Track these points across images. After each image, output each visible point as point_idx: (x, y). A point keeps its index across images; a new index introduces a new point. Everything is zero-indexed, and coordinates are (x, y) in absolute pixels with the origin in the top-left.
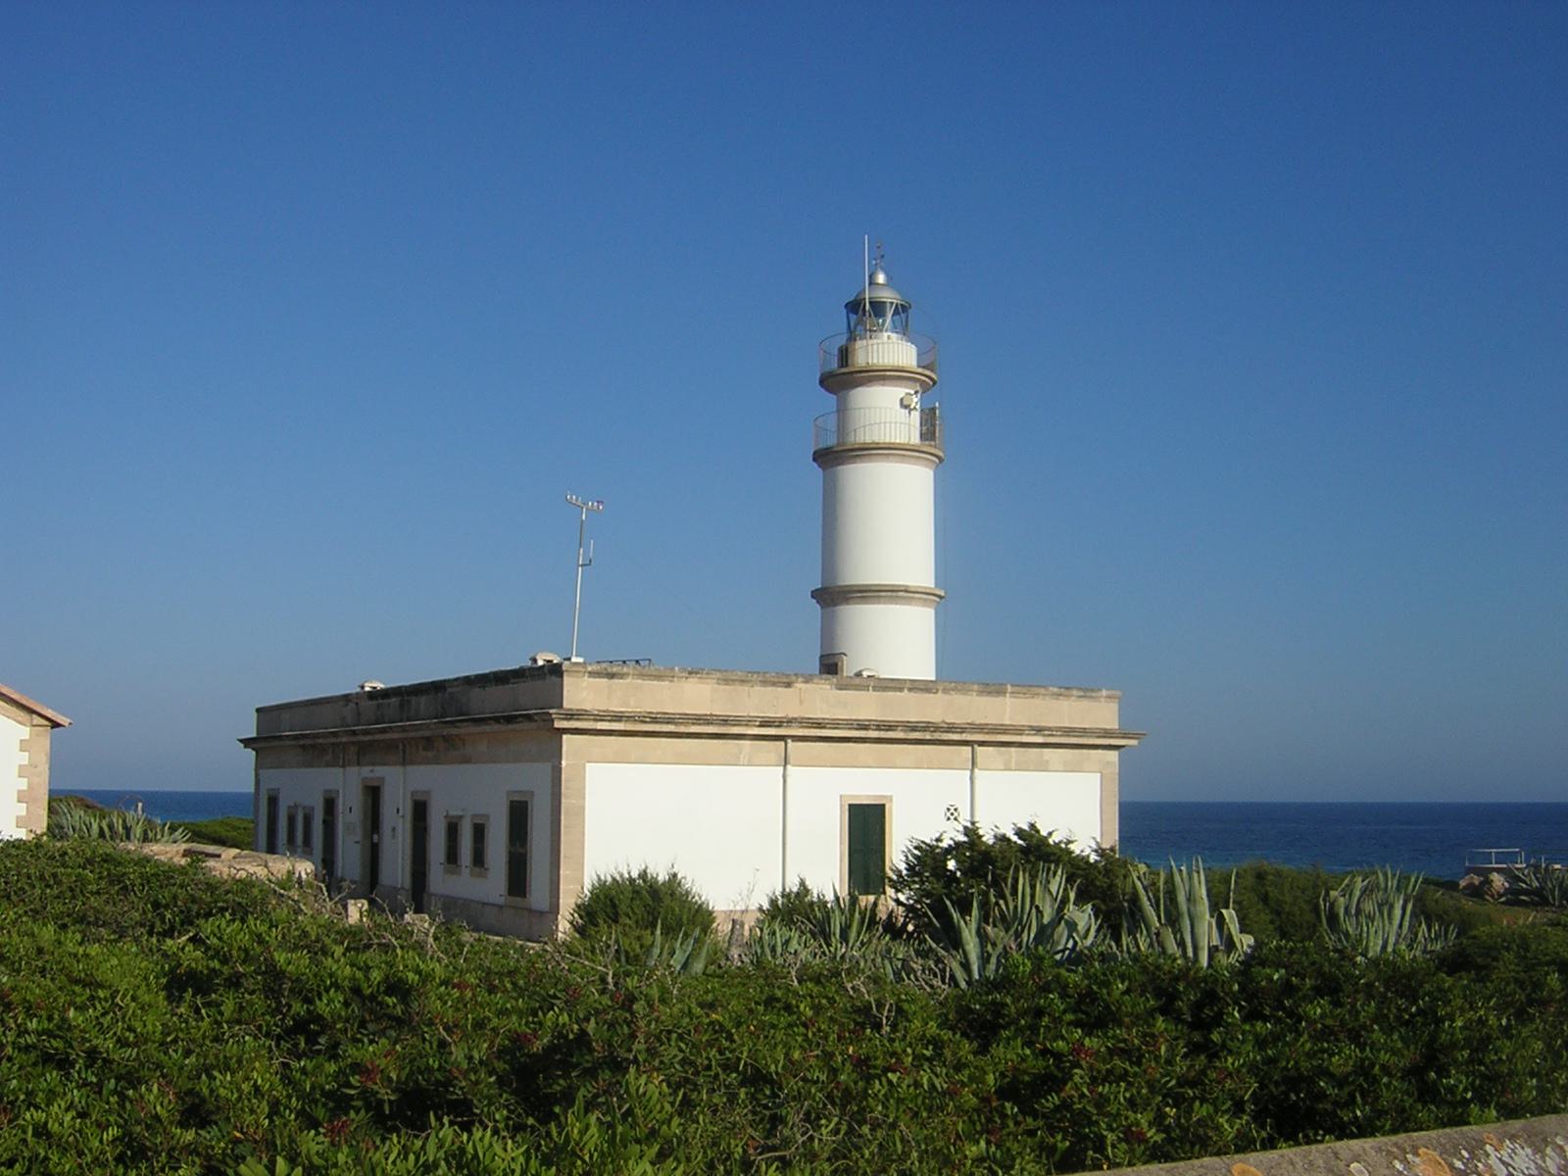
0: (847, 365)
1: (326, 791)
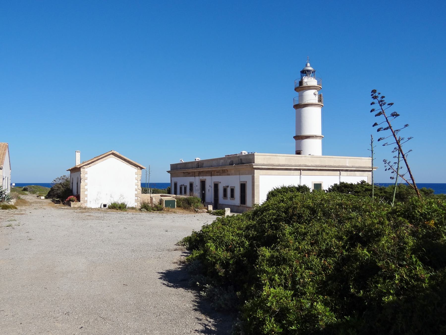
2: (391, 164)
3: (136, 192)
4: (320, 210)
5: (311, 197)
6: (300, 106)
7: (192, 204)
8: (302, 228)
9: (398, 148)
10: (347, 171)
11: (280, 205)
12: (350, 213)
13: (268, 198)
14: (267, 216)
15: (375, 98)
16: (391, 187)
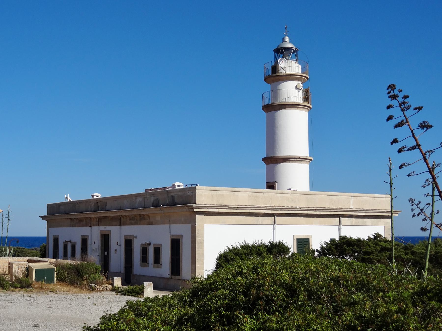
0: (275, 73)
1: (82, 236)
2: (421, 206)
4: (302, 289)
5: (288, 267)
6: (273, 107)
7: (85, 276)
8: (272, 321)
9: (432, 180)
10: (351, 216)
11: (236, 281)
12: (353, 293)
13: (219, 266)
14: (213, 300)
15: (393, 97)
16: (422, 244)
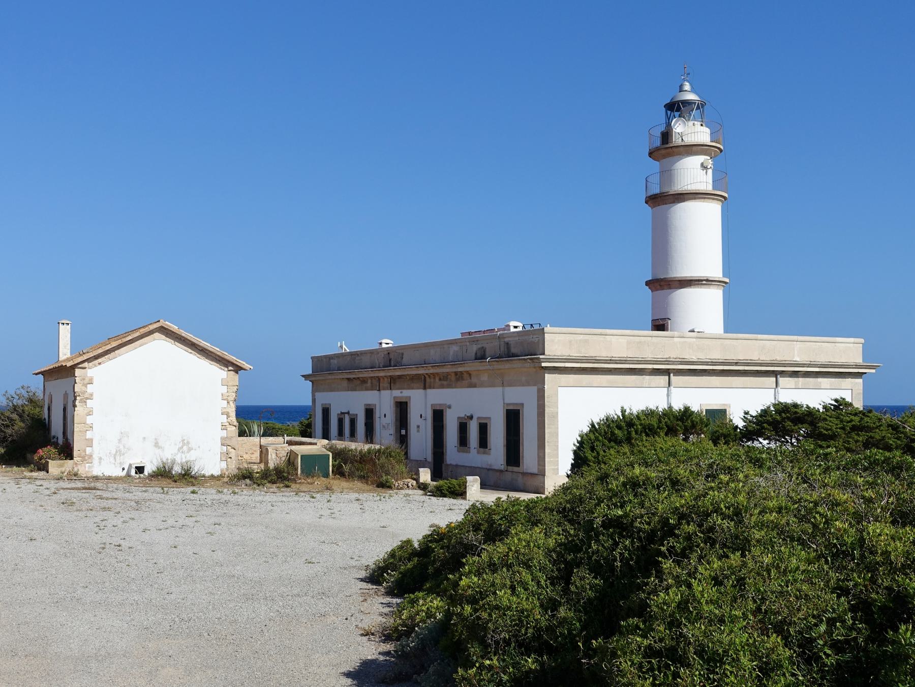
3: (224, 434)
6: (663, 199)
10: (795, 374)
